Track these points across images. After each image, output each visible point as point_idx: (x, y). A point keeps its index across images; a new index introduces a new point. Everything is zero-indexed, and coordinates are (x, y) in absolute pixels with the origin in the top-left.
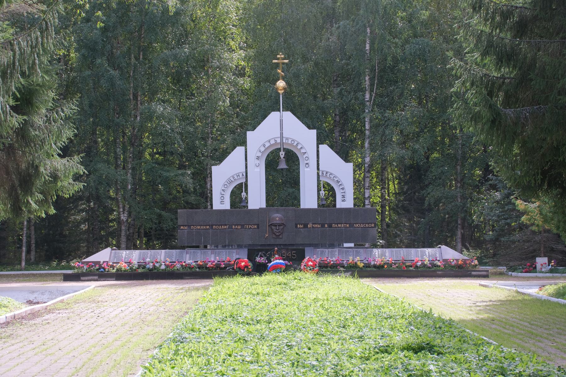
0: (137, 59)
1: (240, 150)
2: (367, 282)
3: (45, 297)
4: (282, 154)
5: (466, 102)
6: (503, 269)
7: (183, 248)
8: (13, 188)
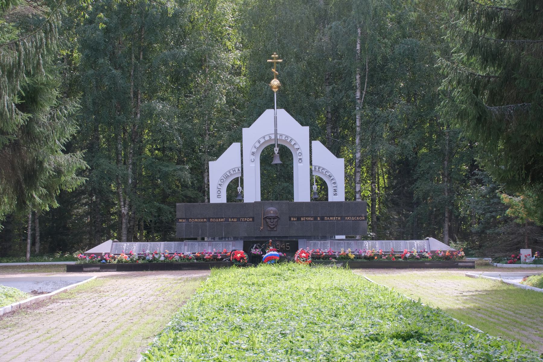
0: (137, 58)
1: (235, 146)
2: (358, 273)
3: (49, 288)
4: (276, 150)
5: (452, 100)
6: (489, 260)
7: (181, 240)
8: (18, 182)
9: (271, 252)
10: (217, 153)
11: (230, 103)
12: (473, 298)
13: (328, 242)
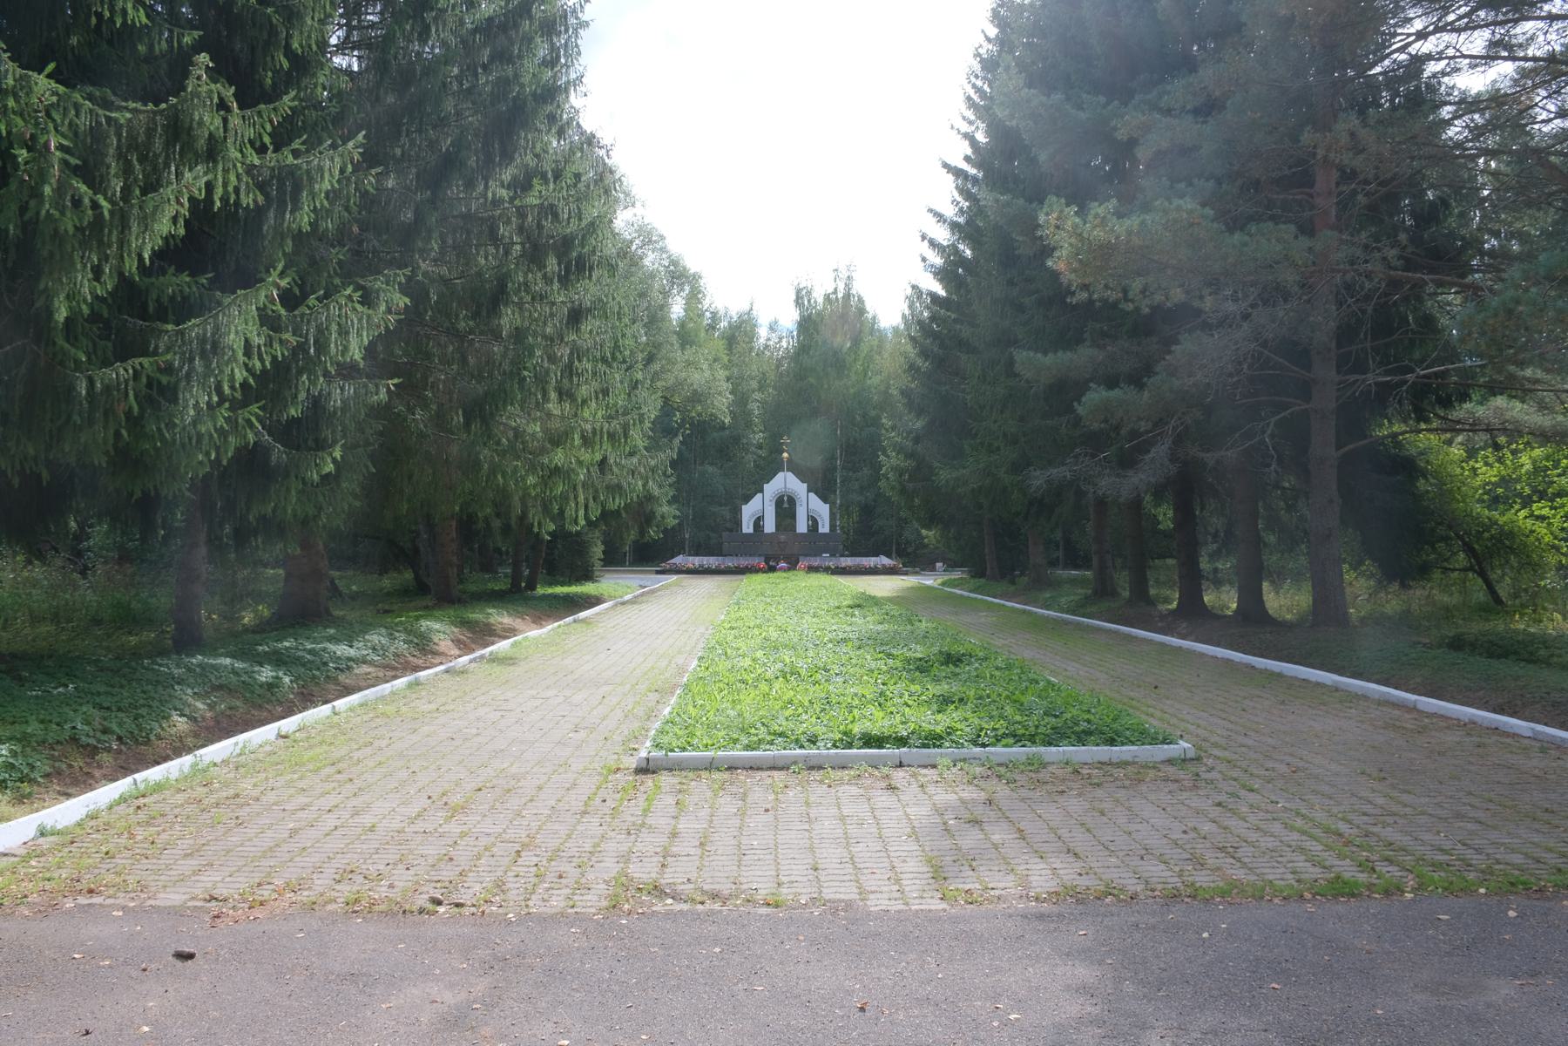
1: (759, 496)
2: (834, 577)
3: (649, 583)
4: (785, 498)
5: (888, 479)
6: (918, 569)
9: (783, 564)
10: (747, 499)
11: (757, 466)
12: (898, 591)
13: (818, 559)
